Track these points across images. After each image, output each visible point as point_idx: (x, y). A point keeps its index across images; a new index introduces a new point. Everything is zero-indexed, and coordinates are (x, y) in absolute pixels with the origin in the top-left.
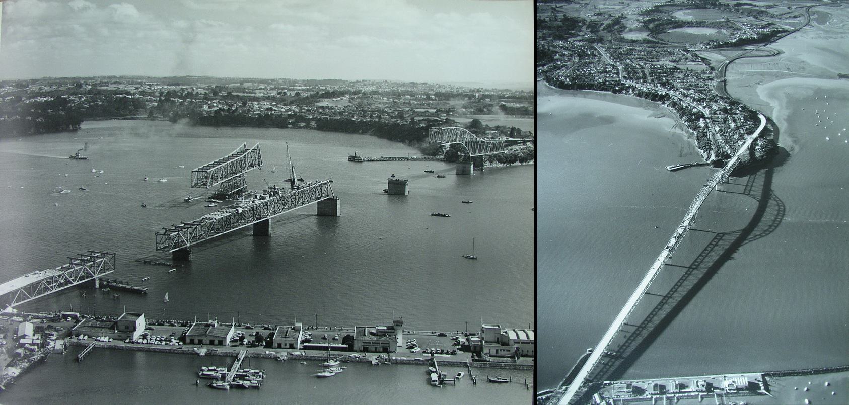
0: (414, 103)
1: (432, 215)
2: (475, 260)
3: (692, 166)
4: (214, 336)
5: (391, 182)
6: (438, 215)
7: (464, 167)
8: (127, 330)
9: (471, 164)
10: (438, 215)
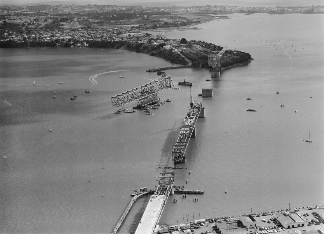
0: (112, 22)
1: (247, 111)
2: (310, 143)
3: (271, 12)
4: (299, 222)
5: (203, 91)
6: (250, 110)
7: (215, 73)
8: (251, 227)
9: (219, 72)
10: (250, 110)
